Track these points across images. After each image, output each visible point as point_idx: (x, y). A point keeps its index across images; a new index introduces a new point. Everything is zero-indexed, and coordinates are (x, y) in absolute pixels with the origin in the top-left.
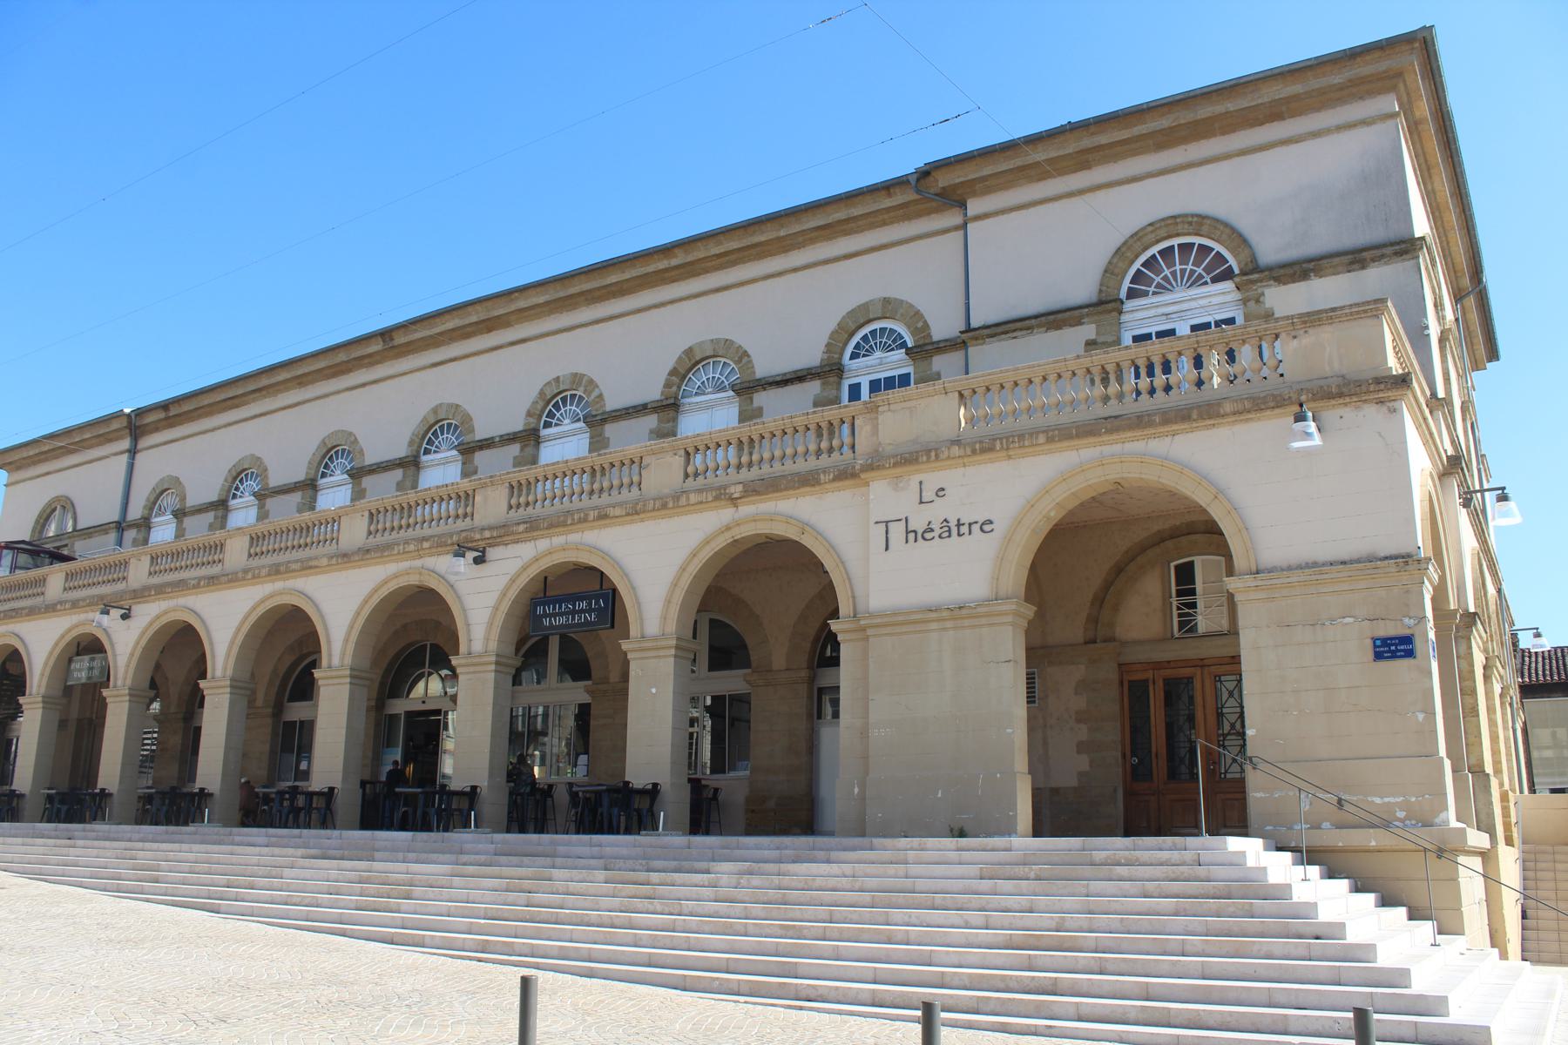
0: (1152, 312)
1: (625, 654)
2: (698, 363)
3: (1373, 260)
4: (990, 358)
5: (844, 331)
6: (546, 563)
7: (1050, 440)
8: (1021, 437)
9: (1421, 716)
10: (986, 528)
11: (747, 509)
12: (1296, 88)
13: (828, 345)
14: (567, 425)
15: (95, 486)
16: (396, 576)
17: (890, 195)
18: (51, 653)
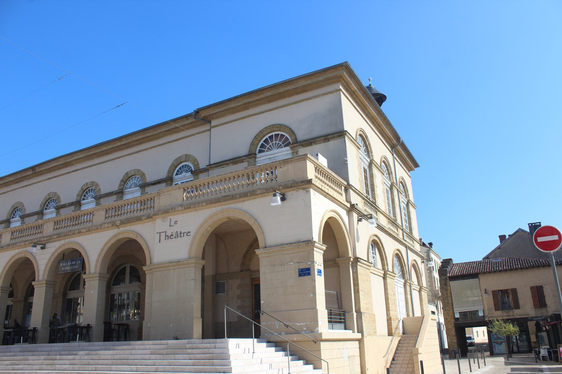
0: (265, 158)
1: (145, 272)
2: (130, 177)
3: (331, 138)
4: (215, 173)
5: (174, 166)
6: (63, 249)
7: (207, 204)
8: (199, 203)
9: (312, 295)
10: (188, 234)
11: (122, 229)
12: (309, 82)
13: (169, 171)
14: (90, 199)
16: (18, 254)
17: (187, 119)
18: (99, 255)
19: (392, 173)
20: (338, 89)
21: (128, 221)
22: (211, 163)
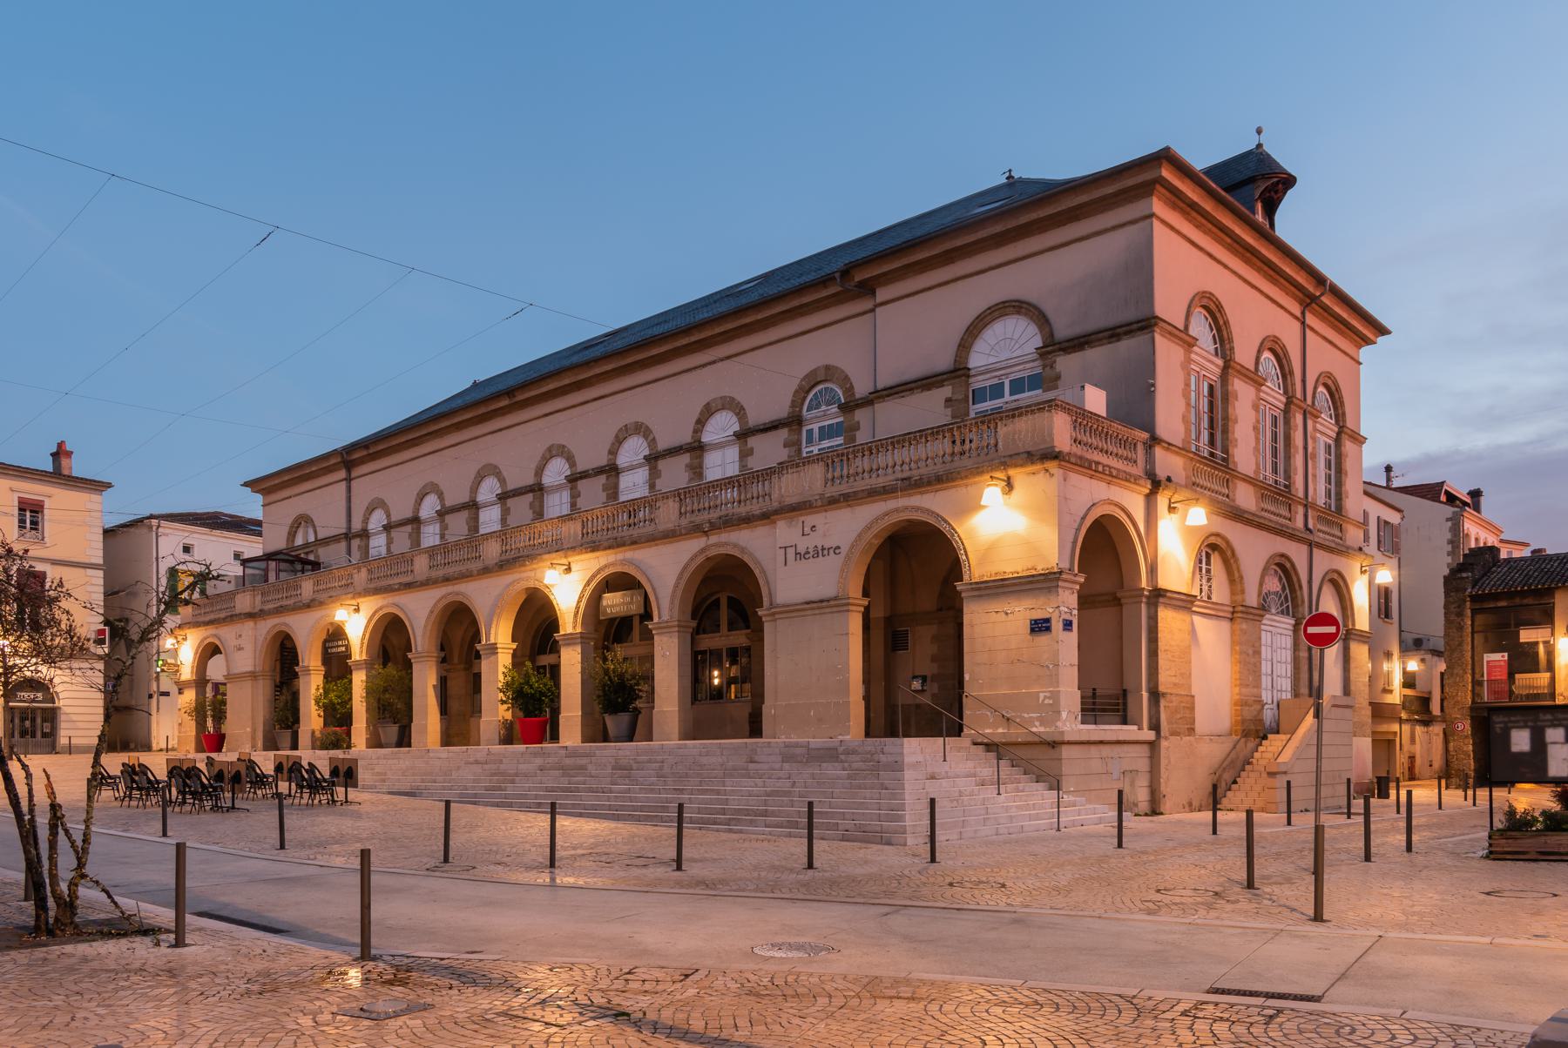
11: (714, 539)
15: (326, 507)
19: (1291, 373)
20: (1147, 213)
21: (729, 523)
22: (880, 386)
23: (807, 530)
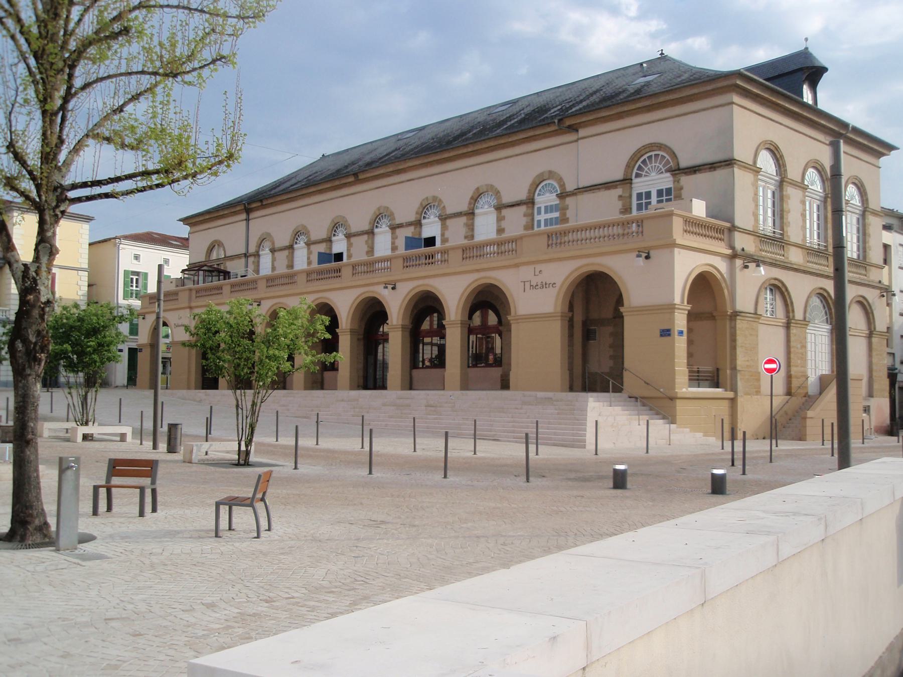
20: (729, 101)
23: (537, 273)
